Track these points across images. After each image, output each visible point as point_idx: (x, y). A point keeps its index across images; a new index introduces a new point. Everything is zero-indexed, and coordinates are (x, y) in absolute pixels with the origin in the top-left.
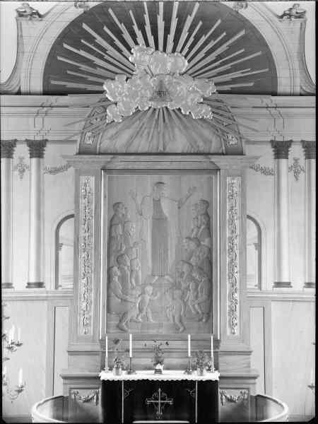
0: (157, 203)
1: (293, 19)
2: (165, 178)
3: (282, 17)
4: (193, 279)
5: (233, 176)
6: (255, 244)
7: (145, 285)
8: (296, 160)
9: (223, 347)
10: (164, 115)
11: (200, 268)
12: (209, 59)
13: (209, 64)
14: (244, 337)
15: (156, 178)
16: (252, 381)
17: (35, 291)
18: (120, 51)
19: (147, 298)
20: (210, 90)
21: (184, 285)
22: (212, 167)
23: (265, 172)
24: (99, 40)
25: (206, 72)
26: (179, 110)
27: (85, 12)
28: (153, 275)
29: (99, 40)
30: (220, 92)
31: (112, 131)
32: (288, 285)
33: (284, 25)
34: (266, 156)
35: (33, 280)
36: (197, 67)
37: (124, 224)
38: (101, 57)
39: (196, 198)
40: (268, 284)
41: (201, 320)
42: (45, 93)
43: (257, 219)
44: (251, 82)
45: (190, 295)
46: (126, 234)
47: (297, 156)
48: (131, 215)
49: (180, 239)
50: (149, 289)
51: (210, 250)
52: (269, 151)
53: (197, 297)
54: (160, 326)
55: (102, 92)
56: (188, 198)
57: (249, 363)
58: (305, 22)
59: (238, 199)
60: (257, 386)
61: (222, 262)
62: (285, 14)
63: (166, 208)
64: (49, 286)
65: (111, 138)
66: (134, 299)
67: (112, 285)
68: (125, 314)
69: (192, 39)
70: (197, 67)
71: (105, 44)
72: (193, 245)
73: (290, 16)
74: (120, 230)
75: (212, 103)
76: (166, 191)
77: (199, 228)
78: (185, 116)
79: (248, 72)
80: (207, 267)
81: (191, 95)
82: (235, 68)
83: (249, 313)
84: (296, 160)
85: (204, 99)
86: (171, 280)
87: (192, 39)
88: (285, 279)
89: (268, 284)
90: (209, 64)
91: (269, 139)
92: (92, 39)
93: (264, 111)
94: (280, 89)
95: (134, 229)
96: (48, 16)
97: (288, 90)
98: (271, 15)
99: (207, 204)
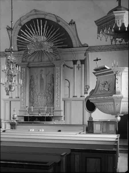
0: (41, 75)
1: (73, 25)
2: (43, 69)
3: (69, 24)
4: (49, 94)
5: (58, 67)
6: (68, 87)
7: (38, 95)
8: (79, 65)
9: (55, 109)
10: (41, 53)
11: (51, 91)
12: (52, 36)
13: (52, 38)
14: (60, 107)
15: (40, 69)
16: (61, 118)
17: (18, 99)
18: (30, 36)
19: (39, 99)
20: (52, 45)
21: (47, 95)
22: (51, 65)
23: (71, 68)
24: (25, 34)
25: (52, 39)
26: (45, 50)
27: (22, 27)
28: (40, 93)
29: (25, 34)
30: (55, 45)
31: (29, 58)
32: (76, 97)
33: (70, 27)
34: (71, 64)
35: (17, 96)
36: (49, 39)
37: (33, 80)
38: (26, 38)
39: (50, 74)
40: (71, 97)
41: (51, 104)
42: (19, 51)
43: (68, 80)
44: (66, 45)
45: (49, 98)
46: (34, 83)
47: (79, 64)
48: (35, 78)
49: (46, 84)
50: (39, 96)
51: (54, 86)
52: (72, 63)
53: (50, 98)
54: (42, 105)
55: (27, 47)
56: (48, 74)
57: (61, 113)
58: (76, 25)
59: (59, 72)
60: (62, 119)
61: (56, 88)
62: (70, 23)
63: (43, 76)
64: (20, 97)
65: (30, 59)
66: (36, 99)
67: (31, 96)
68: (33, 103)
69: (46, 31)
70: (49, 39)
71: (27, 35)
72: (49, 86)
73: (71, 23)
74: (32, 82)
75: (53, 48)
76: (43, 72)
77: (51, 81)
78: (46, 52)
79: (62, 39)
80: (53, 91)
81: (48, 47)
82: (58, 39)
83: (99, 124)
84: (79, 65)
85: (51, 47)
86: (44, 94)
87: (46, 31)
88: (75, 95)
89: (71, 97)
90: (52, 38)
91: (72, 60)
92: (23, 34)
93: (71, 52)
94: (74, 46)
95: (36, 82)
96: (14, 29)
97: (76, 46)
98: (67, 24)
99: (53, 75)
